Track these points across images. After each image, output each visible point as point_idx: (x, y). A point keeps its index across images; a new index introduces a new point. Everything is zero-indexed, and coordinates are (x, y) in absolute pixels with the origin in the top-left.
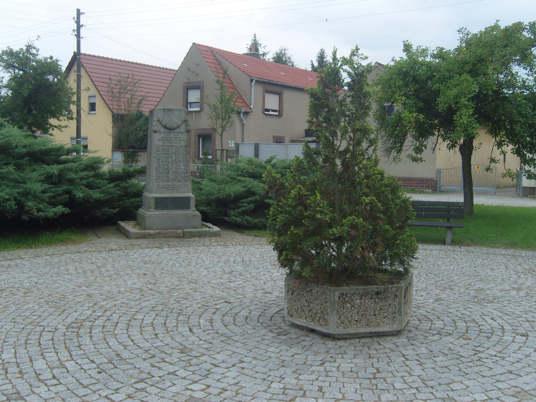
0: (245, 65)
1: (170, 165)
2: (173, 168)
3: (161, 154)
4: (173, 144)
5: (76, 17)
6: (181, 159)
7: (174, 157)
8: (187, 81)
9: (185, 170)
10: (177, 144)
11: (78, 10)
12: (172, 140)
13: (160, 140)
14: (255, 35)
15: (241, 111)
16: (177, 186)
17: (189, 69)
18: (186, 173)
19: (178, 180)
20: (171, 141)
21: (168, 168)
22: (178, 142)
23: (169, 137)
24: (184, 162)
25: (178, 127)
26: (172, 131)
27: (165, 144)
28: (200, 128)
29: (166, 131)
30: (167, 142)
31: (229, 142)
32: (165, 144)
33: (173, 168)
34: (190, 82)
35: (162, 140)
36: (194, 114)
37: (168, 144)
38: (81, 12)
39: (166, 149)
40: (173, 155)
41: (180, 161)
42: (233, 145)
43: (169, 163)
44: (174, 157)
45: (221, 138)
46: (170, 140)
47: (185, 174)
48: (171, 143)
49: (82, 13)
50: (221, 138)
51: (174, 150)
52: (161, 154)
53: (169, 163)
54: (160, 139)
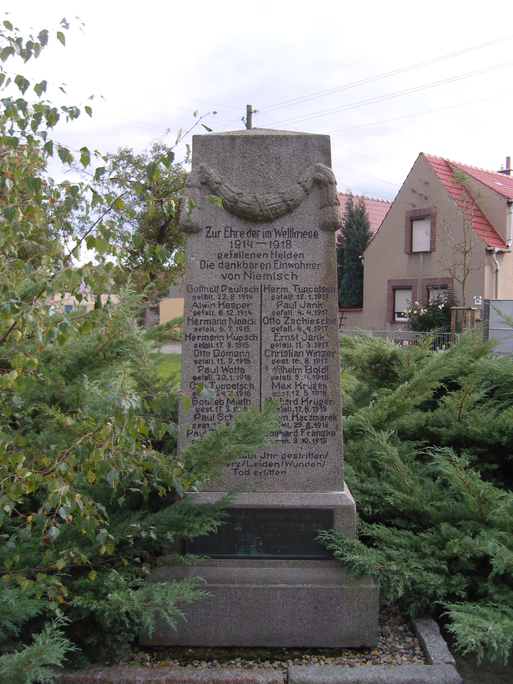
0: (497, 183)
1: (253, 371)
2: (267, 384)
3: (215, 322)
4: (266, 282)
5: (246, 117)
6: (299, 345)
7: (269, 337)
8: (411, 208)
9: (315, 393)
10: (284, 284)
11: (249, 107)
12: (262, 266)
13: (211, 266)
14: (508, 159)
15: (493, 250)
16: (278, 460)
17: (414, 191)
18: (320, 405)
19: (288, 434)
20: (258, 270)
21: (244, 381)
22: (289, 271)
23: (249, 250)
24: (311, 359)
25: (289, 211)
26: (261, 228)
27: (230, 284)
28: (429, 277)
29: (238, 226)
30: (240, 271)
31: (475, 298)
32: (230, 284)
33: (267, 384)
34: (416, 210)
35: (221, 265)
36: (421, 255)
37: (247, 283)
38: (253, 109)
39: (238, 301)
40: (267, 328)
41: (297, 354)
42: (480, 303)
43: (247, 361)
44: (269, 337)
45: (463, 287)
46: (253, 266)
47: (316, 409)
48: (258, 277)
49: (255, 111)
50: (463, 287)
51: (271, 306)
52: (215, 322)
53: (247, 361)
54: (214, 259)
